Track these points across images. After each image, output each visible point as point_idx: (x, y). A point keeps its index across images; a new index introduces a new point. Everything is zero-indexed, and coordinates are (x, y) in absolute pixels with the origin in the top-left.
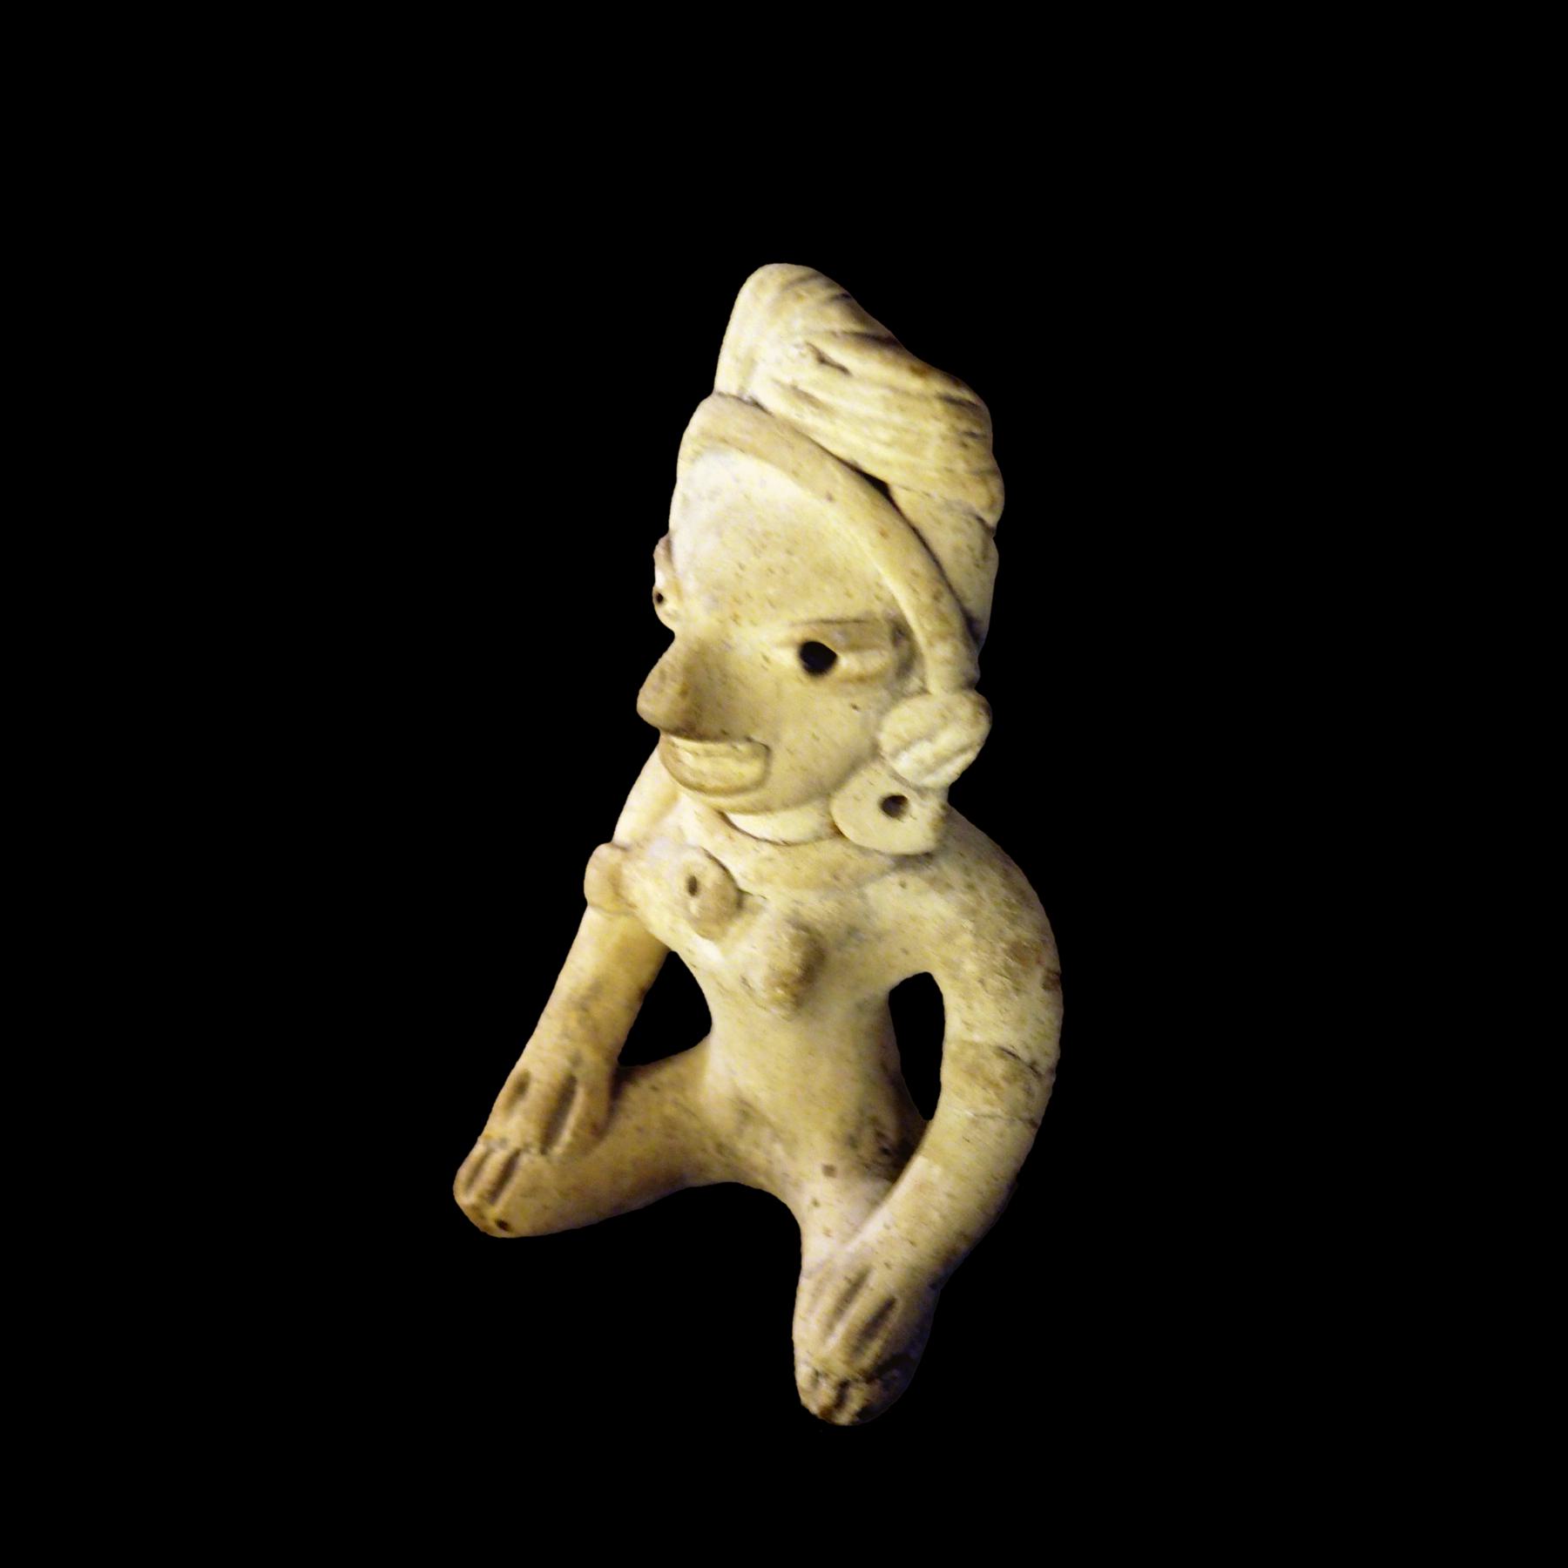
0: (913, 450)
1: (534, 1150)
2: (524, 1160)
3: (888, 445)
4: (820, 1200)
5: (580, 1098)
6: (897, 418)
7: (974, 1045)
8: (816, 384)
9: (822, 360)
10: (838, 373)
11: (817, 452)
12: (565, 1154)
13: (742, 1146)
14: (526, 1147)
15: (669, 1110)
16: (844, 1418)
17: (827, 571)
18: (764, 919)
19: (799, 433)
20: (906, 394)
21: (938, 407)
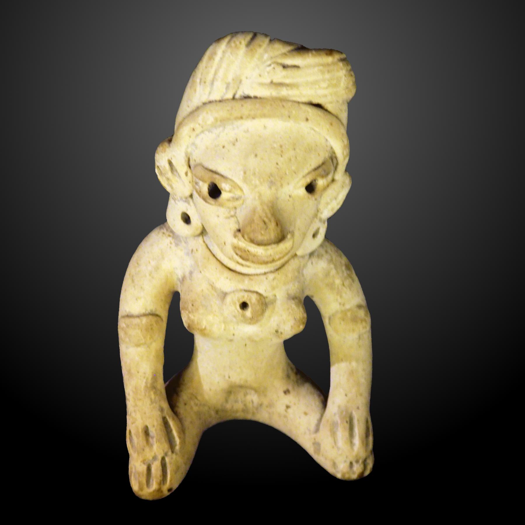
0: (336, 86)
1: (170, 453)
2: (167, 460)
3: (327, 88)
4: (289, 404)
5: (171, 423)
6: (327, 76)
7: (349, 310)
8: (284, 77)
9: (285, 67)
10: (296, 69)
11: (296, 105)
12: (181, 448)
13: (228, 406)
14: (166, 454)
15: (195, 409)
16: (367, 473)
17: (310, 149)
18: (278, 303)
19: (283, 100)
20: (328, 65)
21: (341, 64)
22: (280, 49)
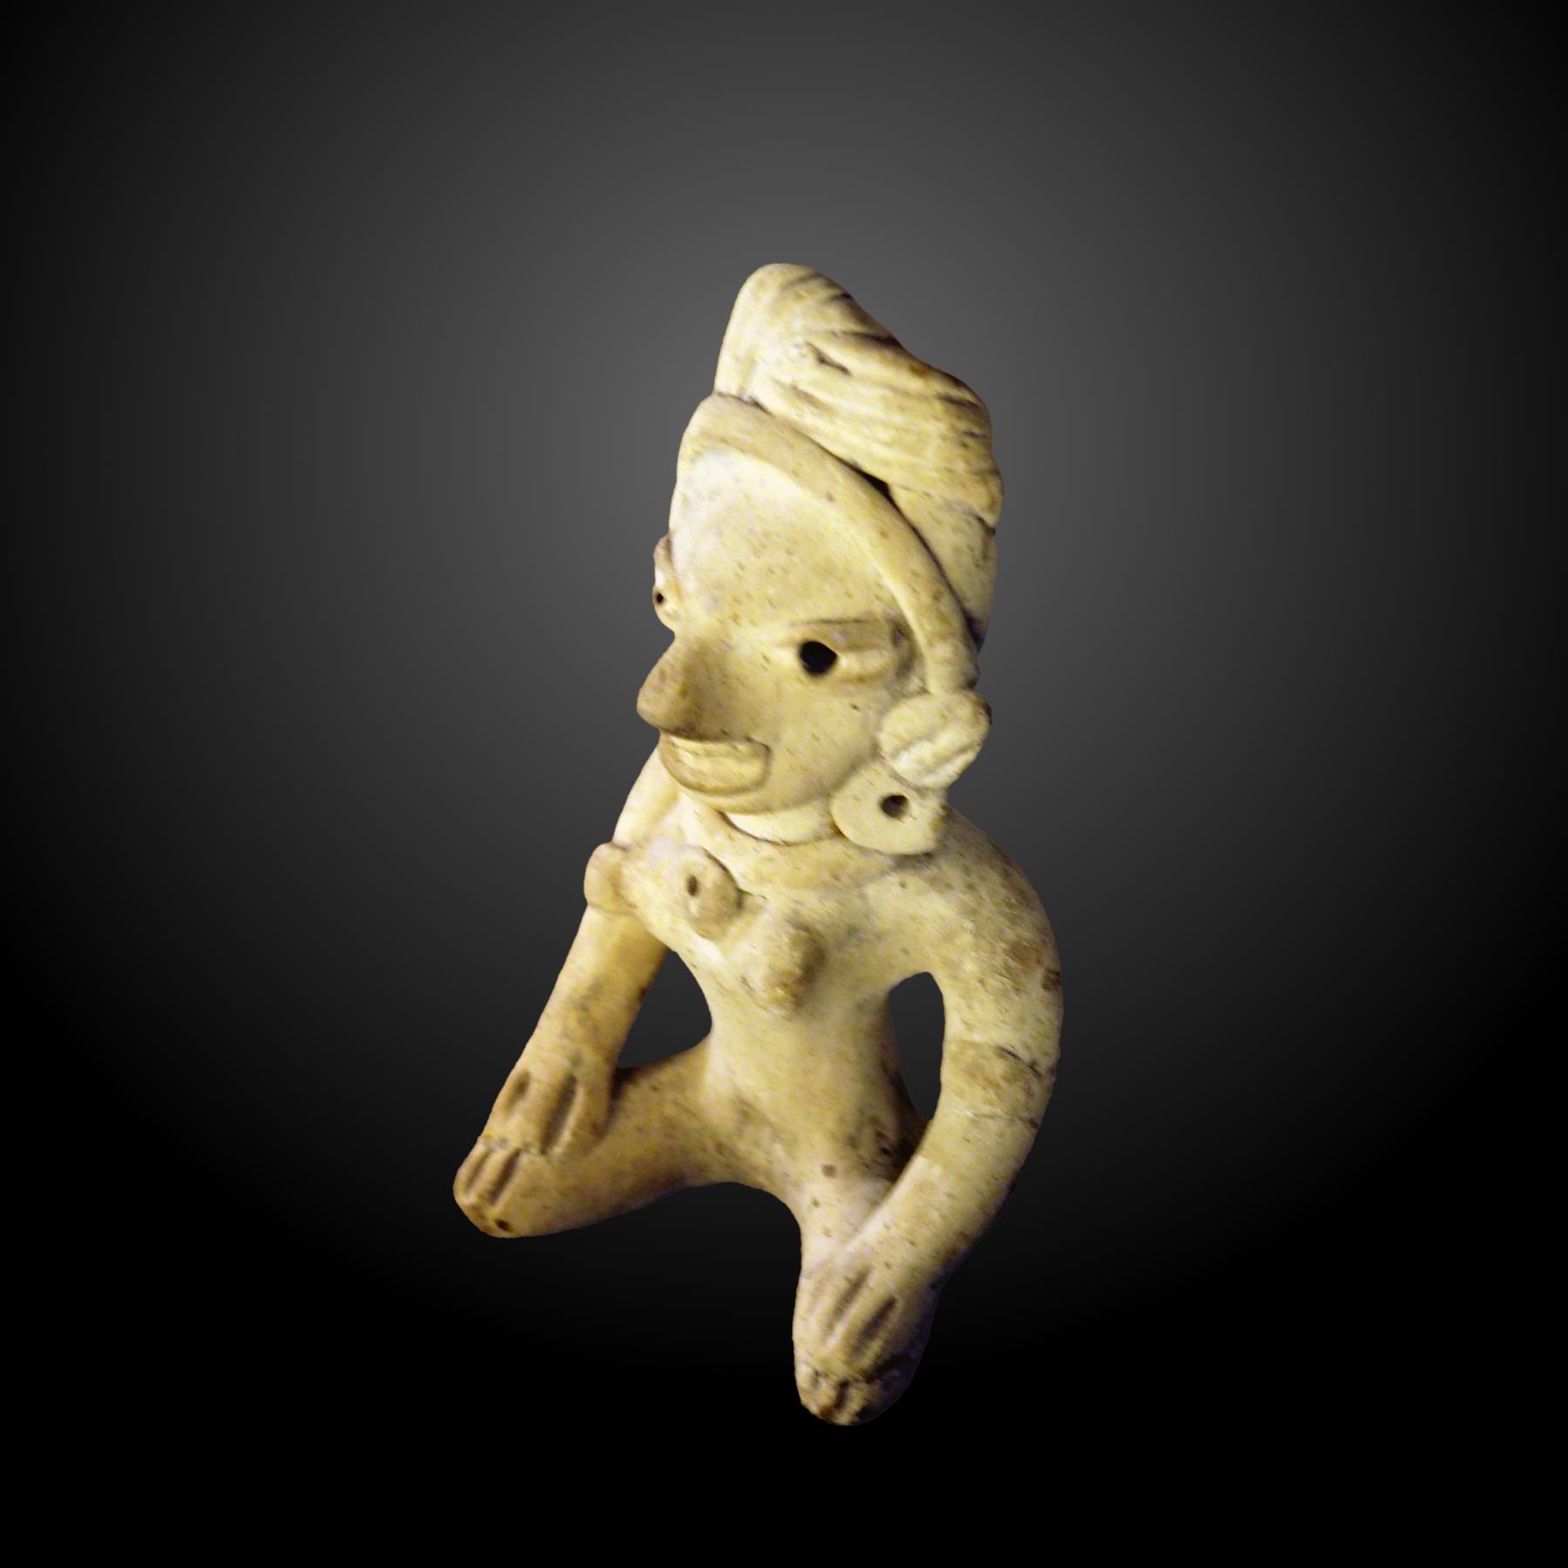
0: (913, 450)
1: (534, 1150)
2: (524, 1160)
3: (888, 445)
4: (820, 1200)
5: (580, 1098)
6: (897, 418)
7: (974, 1045)
8: (816, 384)
9: (822, 360)
10: (838, 373)
11: (817, 452)
12: (565, 1154)
13: (742, 1146)
14: (526, 1147)
15: (669, 1110)
16: (844, 1418)
17: (827, 571)
18: (764, 919)
19: (799, 433)
20: (906, 394)
21: (938, 407)
22: (837, 319)
